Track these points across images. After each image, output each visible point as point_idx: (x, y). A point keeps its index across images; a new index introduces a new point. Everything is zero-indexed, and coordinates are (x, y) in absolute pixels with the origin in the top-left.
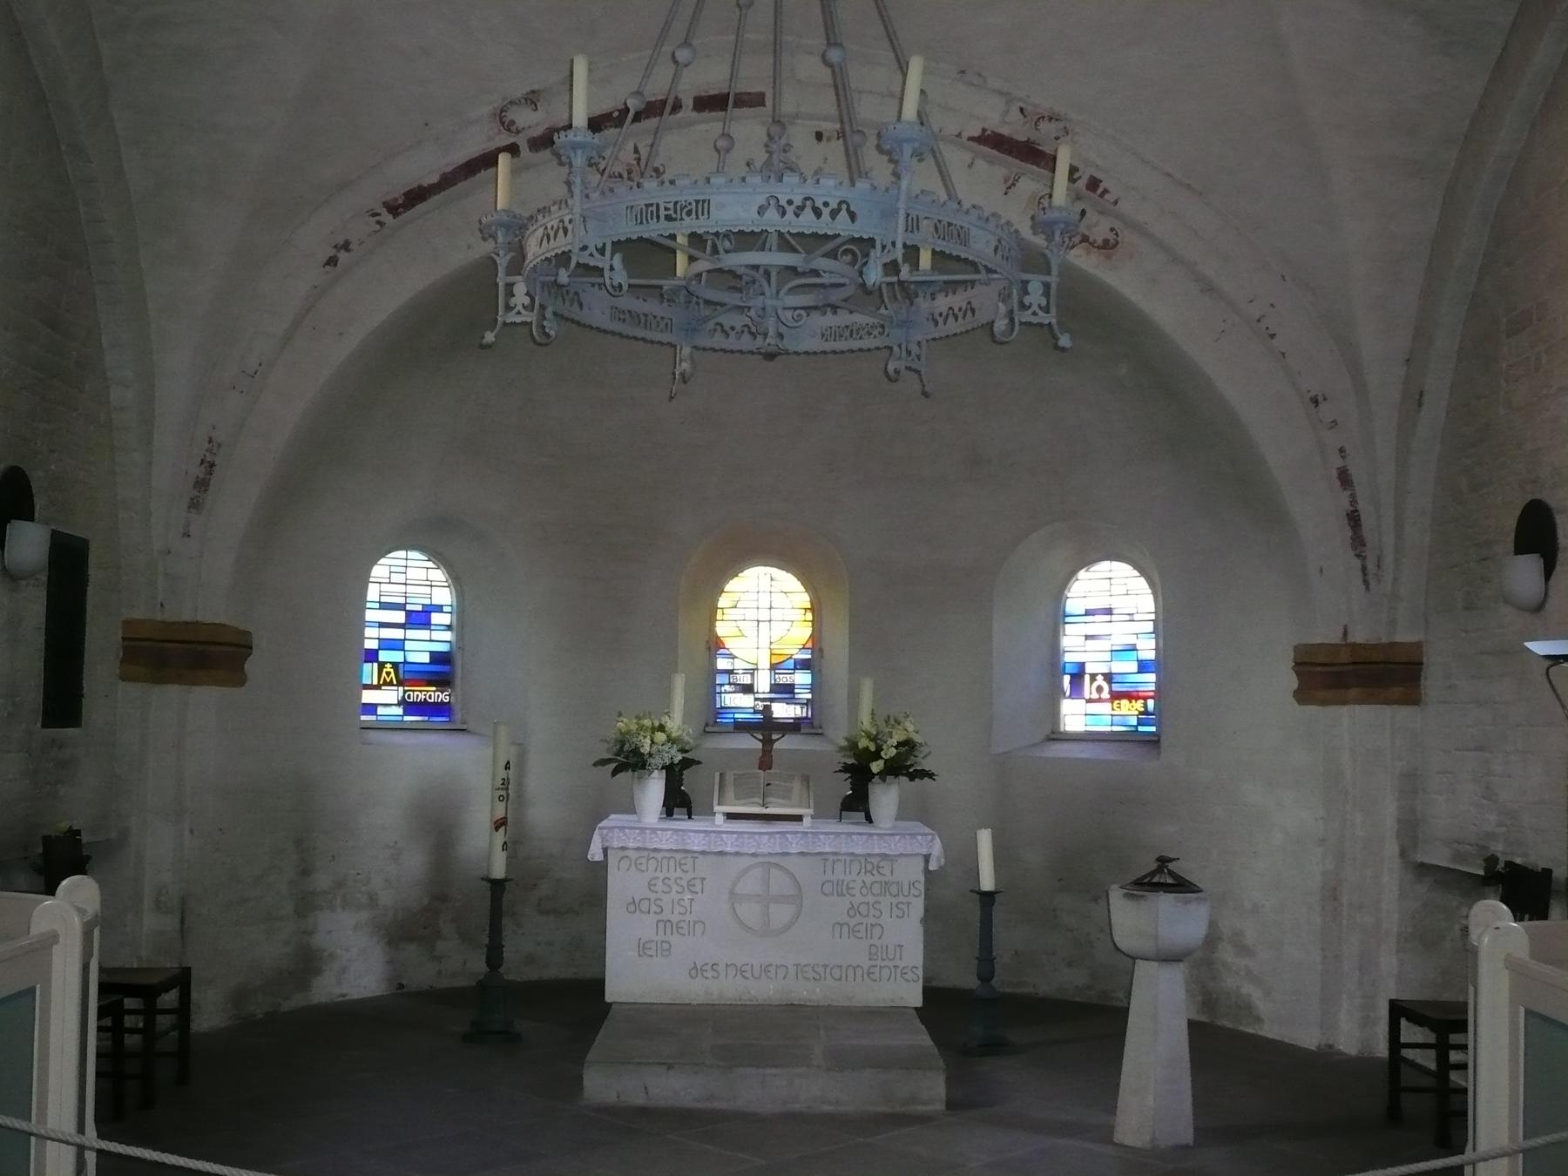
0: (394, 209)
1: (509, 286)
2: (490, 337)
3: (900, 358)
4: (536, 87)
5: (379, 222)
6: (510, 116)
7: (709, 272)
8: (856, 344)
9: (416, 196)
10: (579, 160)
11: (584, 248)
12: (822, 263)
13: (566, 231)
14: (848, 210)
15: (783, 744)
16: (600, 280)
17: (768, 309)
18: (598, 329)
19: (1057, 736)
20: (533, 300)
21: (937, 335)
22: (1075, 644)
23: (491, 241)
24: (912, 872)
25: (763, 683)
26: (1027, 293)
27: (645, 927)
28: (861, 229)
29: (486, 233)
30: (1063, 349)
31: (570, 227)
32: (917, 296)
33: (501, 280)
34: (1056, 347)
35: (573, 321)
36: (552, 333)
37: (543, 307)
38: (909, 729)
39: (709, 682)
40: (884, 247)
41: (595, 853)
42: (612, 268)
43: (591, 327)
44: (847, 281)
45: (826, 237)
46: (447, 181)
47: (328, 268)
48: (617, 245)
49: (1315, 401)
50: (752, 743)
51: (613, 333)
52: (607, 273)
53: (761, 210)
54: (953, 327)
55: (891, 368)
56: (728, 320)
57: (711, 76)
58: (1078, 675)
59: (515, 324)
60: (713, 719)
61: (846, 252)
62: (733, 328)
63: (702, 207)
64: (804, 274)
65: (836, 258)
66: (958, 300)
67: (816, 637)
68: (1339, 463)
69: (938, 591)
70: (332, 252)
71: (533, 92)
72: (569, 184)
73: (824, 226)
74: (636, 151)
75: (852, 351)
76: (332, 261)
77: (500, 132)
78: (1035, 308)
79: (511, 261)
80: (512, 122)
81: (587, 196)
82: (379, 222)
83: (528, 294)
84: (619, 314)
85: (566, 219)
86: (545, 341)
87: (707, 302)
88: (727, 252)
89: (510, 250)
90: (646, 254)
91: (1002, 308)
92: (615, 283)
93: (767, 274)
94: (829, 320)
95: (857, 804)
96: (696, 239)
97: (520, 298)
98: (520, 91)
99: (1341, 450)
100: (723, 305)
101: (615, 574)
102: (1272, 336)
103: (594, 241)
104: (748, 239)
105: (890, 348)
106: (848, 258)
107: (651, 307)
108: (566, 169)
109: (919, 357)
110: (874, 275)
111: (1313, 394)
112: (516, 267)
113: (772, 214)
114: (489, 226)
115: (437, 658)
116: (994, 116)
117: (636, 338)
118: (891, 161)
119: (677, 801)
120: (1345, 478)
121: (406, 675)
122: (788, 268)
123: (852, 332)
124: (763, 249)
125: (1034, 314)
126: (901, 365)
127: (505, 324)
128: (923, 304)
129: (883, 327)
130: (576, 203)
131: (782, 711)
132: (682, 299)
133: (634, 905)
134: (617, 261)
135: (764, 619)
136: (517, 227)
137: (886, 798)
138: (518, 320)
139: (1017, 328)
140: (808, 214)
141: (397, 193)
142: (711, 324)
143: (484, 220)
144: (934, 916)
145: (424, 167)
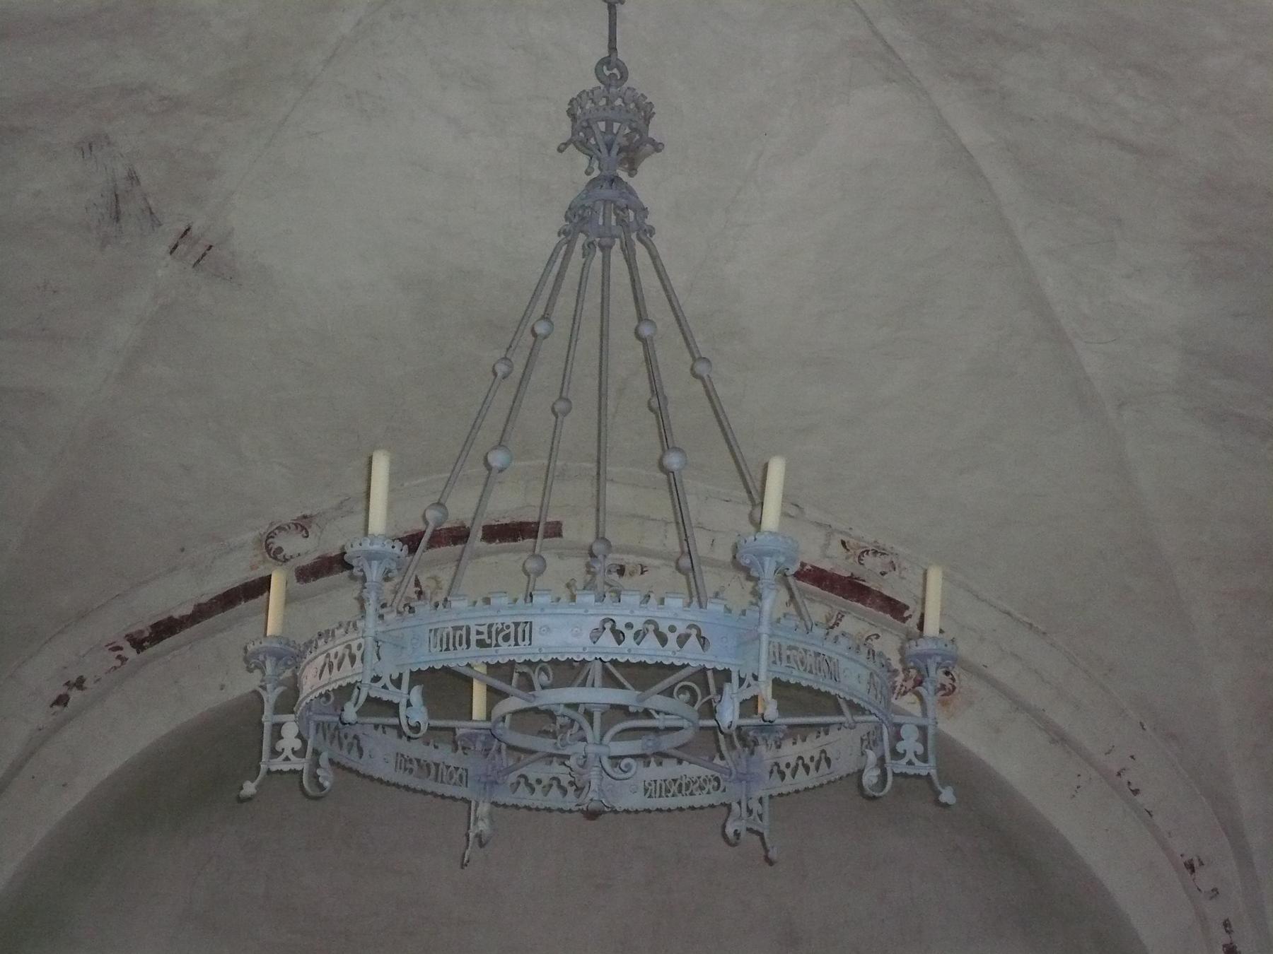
0: (138, 643)
1: (277, 727)
2: (249, 788)
3: (740, 818)
4: (308, 512)
5: (119, 657)
6: (276, 543)
7: (515, 713)
8: (685, 801)
9: (166, 628)
10: (374, 573)
11: (376, 679)
12: (656, 701)
13: (353, 659)
14: (699, 636)
16: (395, 721)
17: (591, 756)
18: (380, 781)
20: (305, 742)
21: (784, 791)
23: (257, 672)
26: (899, 739)
28: (714, 659)
29: (252, 662)
30: (946, 805)
31: (358, 654)
32: (756, 743)
33: (268, 718)
34: (937, 802)
35: (350, 770)
36: (327, 784)
37: (316, 753)
40: (742, 681)
42: (409, 704)
43: (371, 778)
44: (685, 723)
45: (673, 668)
46: (201, 613)
47: (57, 708)
48: (417, 677)
49: (1191, 867)
51: (397, 786)
52: (402, 710)
53: (596, 635)
54: (803, 780)
55: (730, 831)
56: (535, 771)
57: (508, 504)
59: (280, 772)
61: (685, 688)
62: (539, 781)
63: (522, 632)
64: (635, 715)
65: (671, 695)
66: (809, 748)
68: (1225, 939)
70: (63, 690)
71: (305, 517)
72: (361, 601)
73: (669, 654)
74: (417, 583)
75: (680, 809)
76: (62, 700)
77: (264, 561)
78: (910, 756)
79: (281, 695)
80: (280, 549)
81: (381, 617)
82: (119, 657)
83: (299, 736)
84: (404, 762)
85: (354, 645)
86: (318, 795)
87: (511, 748)
88: (543, 688)
89: (280, 684)
90: (444, 687)
91: (872, 756)
92: (412, 723)
93: (589, 715)
94: (655, 772)
96: (499, 670)
97: (290, 740)
98: (289, 514)
99: (1226, 924)
100: (532, 752)
102: (1136, 792)
103: (388, 670)
104: (568, 671)
105: (729, 807)
106: (686, 697)
107: (442, 754)
108: (358, 585)
109: (760, 816)
110: (729, 714)
111: (1186, 859)
112: (288, 703)
113: (607, 640)
114: (255, 654)
117: (424, 792)
118: (749, 578)
122: (615, 707)
123: (684, 787)
124: (583, 684)
125: (910, 763)
126: (741, 826)
127: (269, 772)
128: (766, 754)
129: (717, 779)
130: (371, 625)
132: (479, 746)
134: (416, 695)
136: (291, 656)
138: (286, 767)
139: (890, 778)
140: (651, 642)
141: (142, 623)
142: (513, 778)
143: (251, 648)
145: (177, 596)
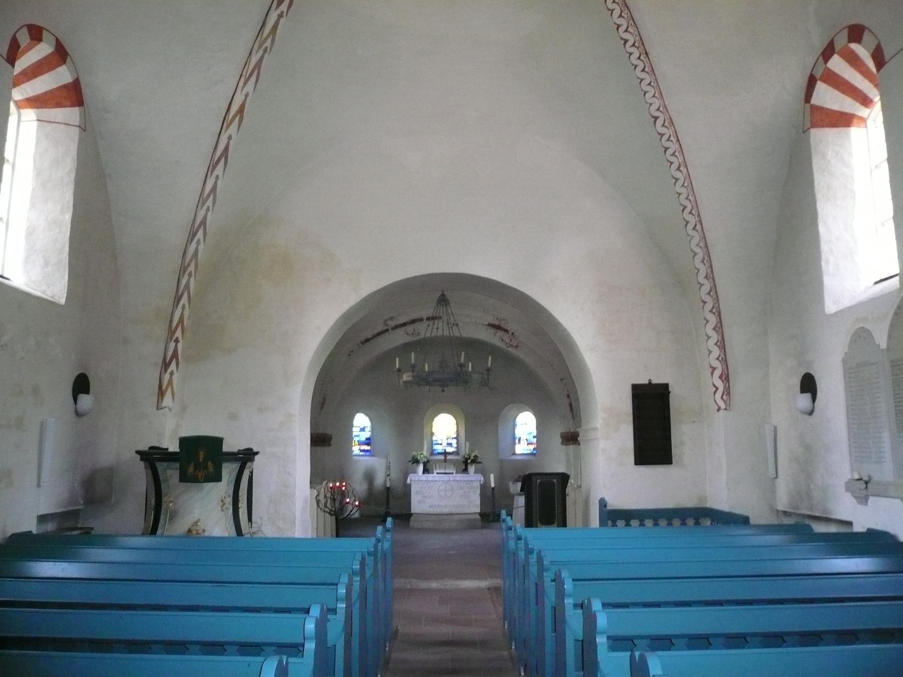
9: (367, 340)
15: (449, 457)
19: (514, 454)
22: (518, 432)
24: (477, 484)
25: (445, 444)
27: (419, 497)
38: (476, 453)
39: (432, 443)
41: (408, 481)
46: (374, 337)
50: (442, 457)
58: (519, 440)
60: (432, 452)
67: (457, 431)
69: (482, 422)
95: (465, 470)
101: (408, 421)
115: (367, 439)
116: (491, 320)
119: (426, 471)
120: (568, 396)
121: (360, 443)
131: (450, 450)
133: (417, 493)
135: (445, 429)
137: (472, 469)
144: (483, 495)
